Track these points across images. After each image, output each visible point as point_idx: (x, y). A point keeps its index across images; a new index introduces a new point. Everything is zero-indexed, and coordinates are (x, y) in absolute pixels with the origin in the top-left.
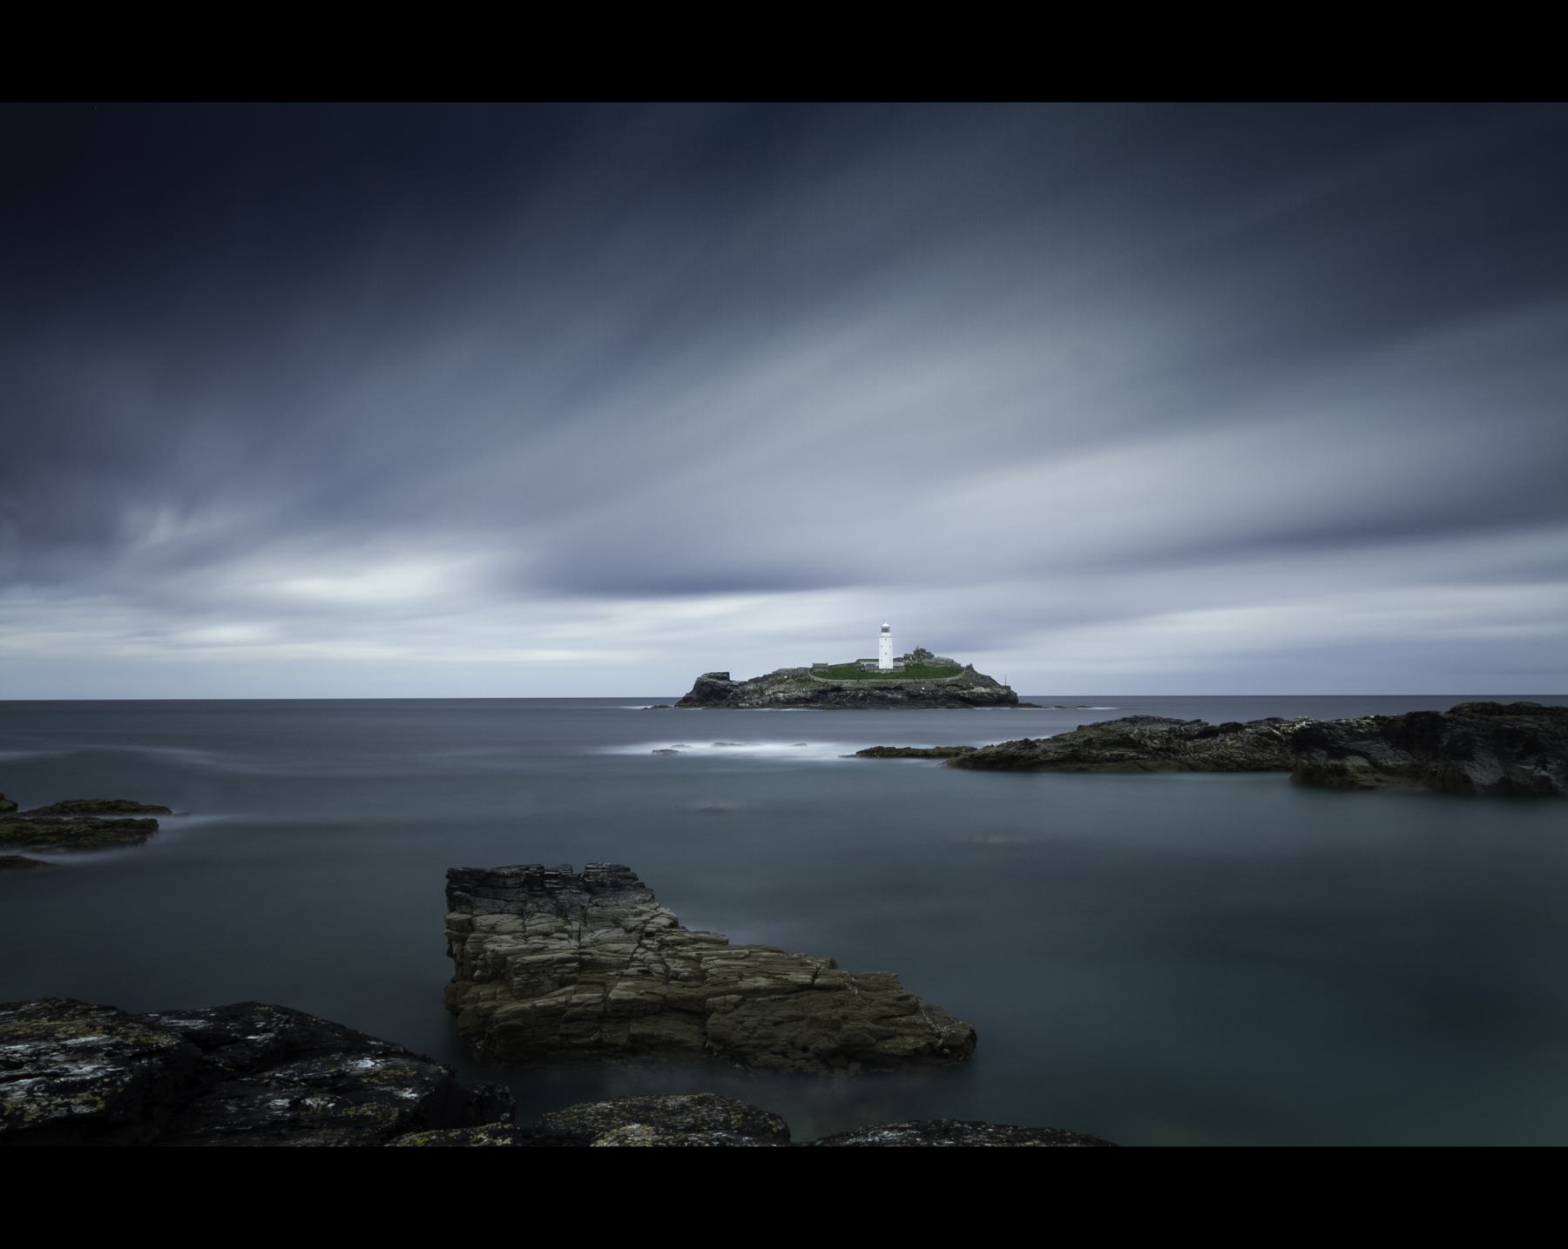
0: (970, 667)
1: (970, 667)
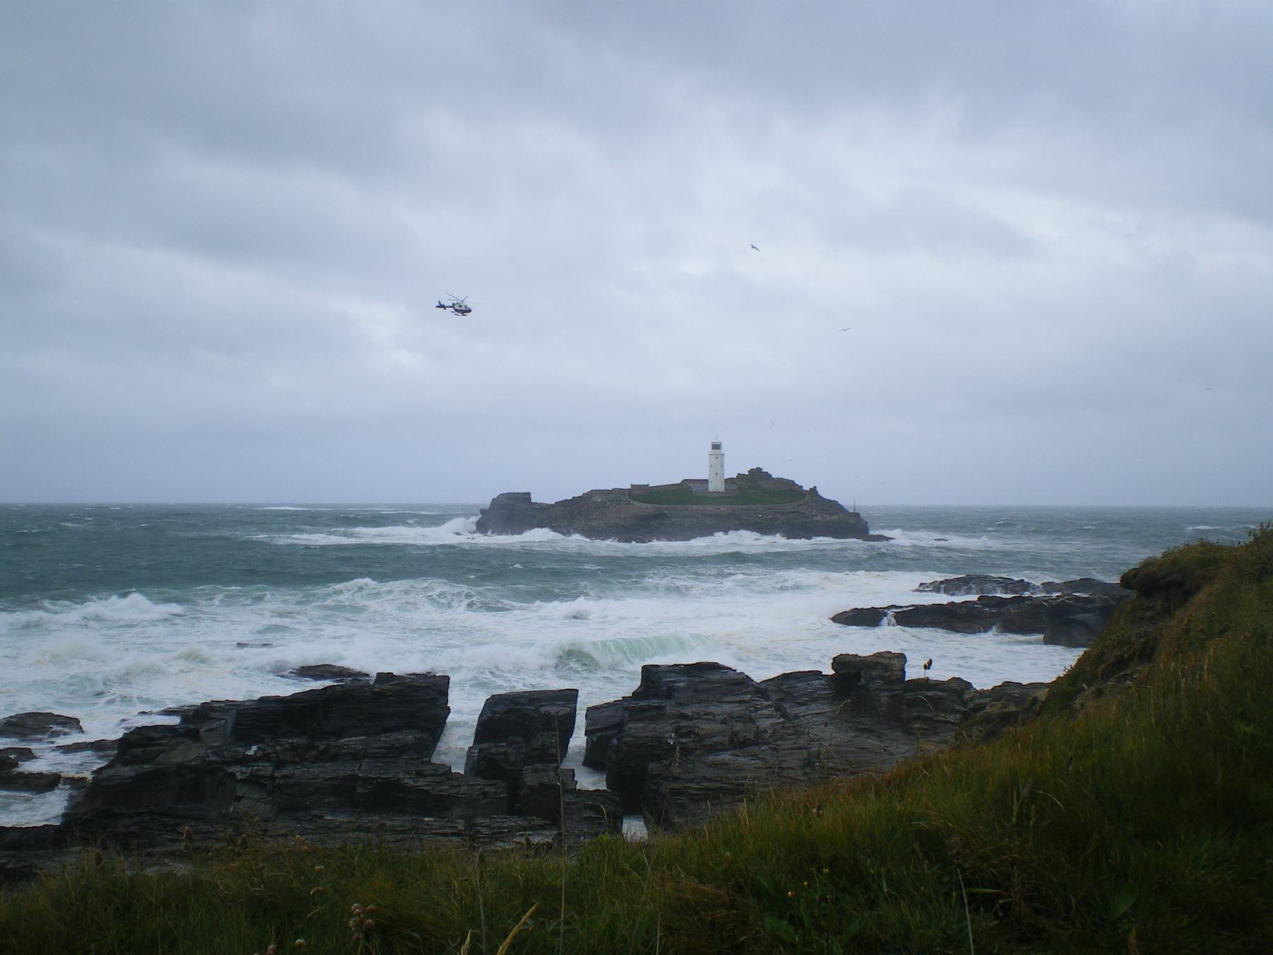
0: (814, 490)
1: (814, 490)
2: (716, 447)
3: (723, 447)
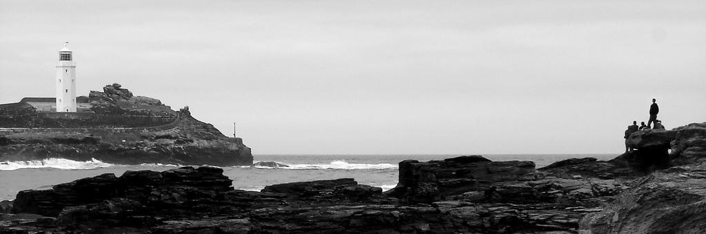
0: (185, 112)
1: (185, 112)
2: (66, 57)
3: (73, 56)
